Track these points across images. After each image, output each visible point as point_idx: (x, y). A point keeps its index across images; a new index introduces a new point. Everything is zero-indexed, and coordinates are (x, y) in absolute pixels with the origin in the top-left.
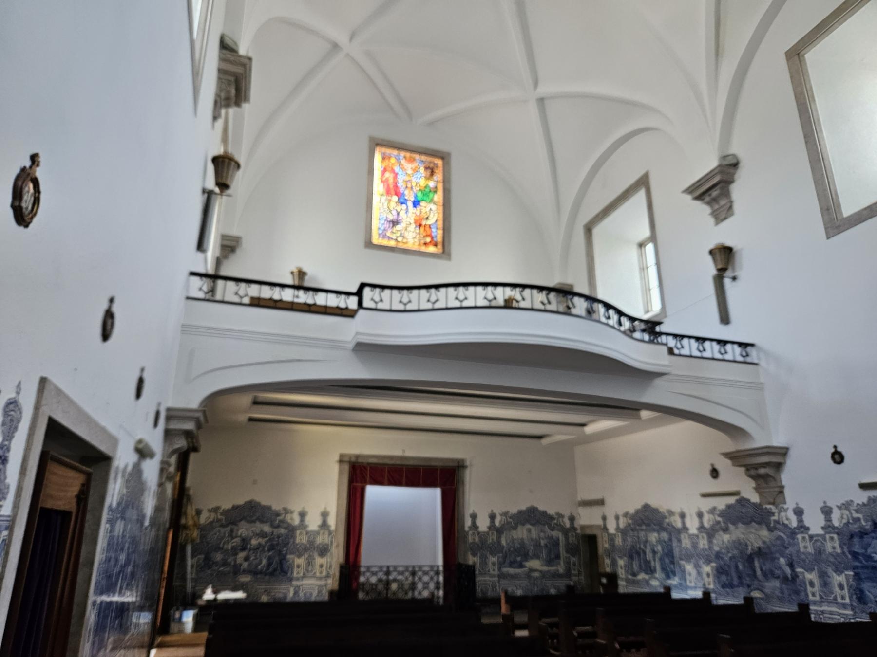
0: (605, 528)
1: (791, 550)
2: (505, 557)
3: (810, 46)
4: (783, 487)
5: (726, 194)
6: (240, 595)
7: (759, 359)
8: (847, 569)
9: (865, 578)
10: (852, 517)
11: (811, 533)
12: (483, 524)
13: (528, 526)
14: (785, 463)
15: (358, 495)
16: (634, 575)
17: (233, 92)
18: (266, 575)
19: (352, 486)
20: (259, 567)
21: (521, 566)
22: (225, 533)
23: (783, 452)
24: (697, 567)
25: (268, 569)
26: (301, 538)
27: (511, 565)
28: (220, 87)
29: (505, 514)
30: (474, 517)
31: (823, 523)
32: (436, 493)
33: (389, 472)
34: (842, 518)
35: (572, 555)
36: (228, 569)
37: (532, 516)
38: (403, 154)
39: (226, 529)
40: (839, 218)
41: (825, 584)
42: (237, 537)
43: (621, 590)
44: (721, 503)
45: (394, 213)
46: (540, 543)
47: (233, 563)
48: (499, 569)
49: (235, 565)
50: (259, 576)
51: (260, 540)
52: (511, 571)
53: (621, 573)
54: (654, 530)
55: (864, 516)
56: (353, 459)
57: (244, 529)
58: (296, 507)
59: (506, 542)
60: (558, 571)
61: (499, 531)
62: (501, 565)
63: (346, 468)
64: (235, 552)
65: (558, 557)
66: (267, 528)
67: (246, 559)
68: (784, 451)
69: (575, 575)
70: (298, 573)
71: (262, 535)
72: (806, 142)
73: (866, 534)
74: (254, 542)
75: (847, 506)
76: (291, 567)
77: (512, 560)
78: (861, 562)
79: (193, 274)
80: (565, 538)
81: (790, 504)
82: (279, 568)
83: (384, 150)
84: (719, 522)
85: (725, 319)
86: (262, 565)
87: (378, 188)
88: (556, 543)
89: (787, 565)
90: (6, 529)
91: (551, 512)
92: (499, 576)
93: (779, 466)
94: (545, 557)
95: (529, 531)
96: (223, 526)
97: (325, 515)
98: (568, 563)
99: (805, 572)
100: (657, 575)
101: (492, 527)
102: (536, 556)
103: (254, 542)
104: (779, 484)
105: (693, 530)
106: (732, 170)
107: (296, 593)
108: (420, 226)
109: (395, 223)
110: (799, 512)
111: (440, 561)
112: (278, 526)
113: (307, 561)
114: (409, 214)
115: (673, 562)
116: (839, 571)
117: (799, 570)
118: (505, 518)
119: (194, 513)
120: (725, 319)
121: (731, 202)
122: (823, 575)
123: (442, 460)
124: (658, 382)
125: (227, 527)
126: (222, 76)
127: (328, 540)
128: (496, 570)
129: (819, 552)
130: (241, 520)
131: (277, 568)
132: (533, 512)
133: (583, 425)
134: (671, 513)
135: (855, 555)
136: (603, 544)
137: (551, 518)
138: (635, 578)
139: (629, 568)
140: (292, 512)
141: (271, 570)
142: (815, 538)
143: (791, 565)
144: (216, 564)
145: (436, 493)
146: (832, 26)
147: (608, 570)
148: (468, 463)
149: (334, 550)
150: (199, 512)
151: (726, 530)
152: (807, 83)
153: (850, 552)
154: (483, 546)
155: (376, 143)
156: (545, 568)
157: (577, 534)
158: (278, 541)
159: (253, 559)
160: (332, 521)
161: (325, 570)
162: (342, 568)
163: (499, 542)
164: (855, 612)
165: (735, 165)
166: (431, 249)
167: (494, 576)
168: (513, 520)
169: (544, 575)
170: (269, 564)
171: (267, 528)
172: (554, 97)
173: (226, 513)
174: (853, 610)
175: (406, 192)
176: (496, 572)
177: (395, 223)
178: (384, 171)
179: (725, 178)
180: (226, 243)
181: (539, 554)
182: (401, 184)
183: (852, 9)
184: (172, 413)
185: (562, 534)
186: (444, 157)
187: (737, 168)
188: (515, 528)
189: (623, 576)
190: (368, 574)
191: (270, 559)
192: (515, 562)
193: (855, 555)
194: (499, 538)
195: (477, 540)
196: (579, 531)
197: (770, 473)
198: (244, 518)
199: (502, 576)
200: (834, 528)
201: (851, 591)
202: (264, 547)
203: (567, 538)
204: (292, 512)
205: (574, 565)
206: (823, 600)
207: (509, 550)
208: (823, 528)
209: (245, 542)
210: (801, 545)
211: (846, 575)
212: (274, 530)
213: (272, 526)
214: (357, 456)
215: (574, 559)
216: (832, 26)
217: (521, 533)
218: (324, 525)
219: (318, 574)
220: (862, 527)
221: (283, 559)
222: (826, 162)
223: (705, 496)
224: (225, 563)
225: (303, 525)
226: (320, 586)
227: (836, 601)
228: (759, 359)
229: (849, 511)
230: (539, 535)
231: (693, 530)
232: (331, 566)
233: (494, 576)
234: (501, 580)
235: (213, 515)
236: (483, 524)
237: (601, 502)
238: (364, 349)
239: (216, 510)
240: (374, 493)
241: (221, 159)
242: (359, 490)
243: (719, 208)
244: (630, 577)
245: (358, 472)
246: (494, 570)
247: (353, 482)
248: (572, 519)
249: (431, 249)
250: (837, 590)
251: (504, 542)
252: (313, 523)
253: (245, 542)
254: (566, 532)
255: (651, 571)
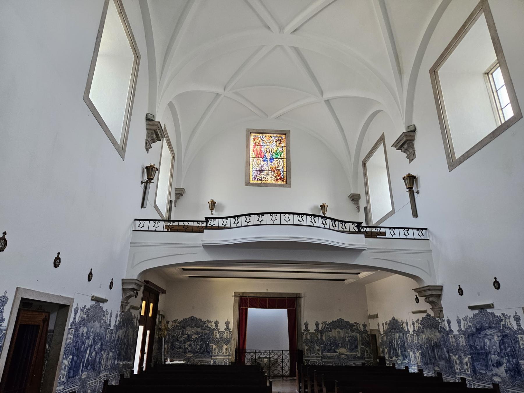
0: (379, 331)
1: (447, 343)
2: (325, 347)
3: (439, 67)
4: (442, 308)
5: (412, 147)
6: (182, 362)
7: (429, 236)
8: (468, 355)
9: (475, 360)
10: (468, 325)
11: (310, 332)
12: (312, 328)
13: (338, 330)
14: (442, 294)
15: (244, 313)
16: (392, 358)
17: (155, 136)
18: (199, 353)
19: (240, 309)
20: (196, 350)
21: (335, 352)
22: (180, 333)
23: (441, 288)
24: (414, 353)
25: (199, 351)
26: (216, 335)
27: (329, 351)
28: (148, 136)
29: (325, 323)
30: (306, 324)
31: (458, 328)
32: (284, 312)
33: (259, 301)
34: (465, 326)
35: (365, 346)
36: (182, 351)
37: (340, 324)
38: (264, 135)
39: (180, 331)
40: (453, 161)
41: (461, 363)
42: (185, 334)
43: (387, 365)
44: (421, 316)
45: (260, 166)
46: (346, 340)
47: (184, 348)
48: (322, 353)
49: (185, 348)
50: (196, 354)
51: (196, 336)
52: (329, 354)
53: (386, 356)
54: (397, 332)
55: (472, 324)
56: (241, 295)
57: (189, 331)
58: (213, 320)
59: (326, 338)
60: (357, 355)
61: (322, 332)
62: (322, 351)
63: (238, 298)
64: (184, 342)
65: (357, 347)
66: (199, 330)
67: (190, 345)
68: (441, 288)
69: (368, 358)
70: (215, 353)
71: (198, 333)
72: (439, 119)
73: (474, 335)
74: (193, 337)
75: (465, 319)
76: (211, 350)
77: (329, 349)
78: (473, 351)
79: (136, 220)
80: (361, 337)
81: (445, 318)
82: (205, 350)
83: (254, 134)
84: (470, 326)
85: (415, 214)
86: (198, 348)
87: (252, 154)
88: (356, 339)
89: (447, 352)
90: (5, 330)
91: (352, 322)
92: (322, 357)
93: (439, 296)
94: (349, 347)
95: (339, 332)
96: (178, 329)
97: (227, 323)
98: (363, 351)
99: (453, 356)
100: (400, 358)
101: (317, 330)
102: (344, 347)
103: (193, 337)
104: (440, 306)
105: (456, 332)
106: (412, 134)
107: (214, 363)
108: (274, 171)
109: (260, 171)
110: (449, 322)
111: (288, 348)
112: (205, 329)
113: (219, 347)
114: (268, 166)
115: (405, 350)
116: (465, 355)
117: (451, 355)
118: (324, 325)
119: (165, 322)
120: (415, 214)
121: (414, 151)
122: (460, 358)
123: (288, 294)
124: (363, 253)
125: (181, 330)
126: (148, 131)
127: (229, 337)
128: (320, 354)
129: (221, 338)
130: (187, 326)
131: (205, 350)
132: (341, 322)
133: (358, 274)
134: (403, 322)
135: (471, 346)
136: (379, 341)
137: (352, 325)
138: (392, 359)
139: (389, 352)
140: (212, 322)
141: (202, 351)
142: (311, 334)
143: (448, 352)
144: (176, 348)
145: (284, 312)
146: (445, 57)
147: (382, 355)
148: (303, 295)
149: (232, 341)
150: (168, 322)
151: (423, 332)
152: (438, 86)
153: (469, 345)
154: (312, 340)
155: (251, 132)
156: (348, 353)
157: (368, 334)
158: (205, 337)
159: (193, 346)
160: (231, 326)
161: (228, 352)
162: (236, 350)
163: (321, 339)
164: (473, 379)
165: (415, 131)
166: (280, 182)
167: (319, 357)
168: (330, 327)
169: (348, 357)
170: (201, 348)
171: (199, 330)
172: (333, 99)
173: (180, 322)
174: (472, 377)
175: (267, 154)
176: (320, 355)
177: (260, 171)
178: (255, 145)
179: (409, 138)
180: (178, 192)
181: (346, 346)
182: (264, 151)
183: (452, 48)
184: (124, 281)
185: (359, 335)
186: (286, 133)
187: (416, 132)
188: (331, 331)
189: (388, 359)
190: (260, 354)
191: (201, 345)
192: (331, 350)
193: (471, 346)
194: (321, 336)
195: (309, 337)
196: (369, 333)
197: (434, 301)
198: (188, 325)
199: (323, 357)
200: (462, 331)
201: (470, 367)
202: (198, 339)
203: (362, 337)
204: (212, 322)
205: (367, 352)
206: (461, 372)
207: (328, 344)
208: (315, 330)
209: (189, 337)
210: (451, 341)
211: (468, 357)
212: (203, 331)
213: (202, 329)
214: (243, 293)
215: (367, 349)
216: (445, 57)
217: (335, 333)
218: (227, 328)
219: (224, 354)
220: (472, 331)
221: (207, 346)
222: (448, 130)
223: (414, 313)
224: (180, 348)
225: (217, 328)
226: (226, 360)
227: (465, 373)
228: (429, 236)
229: (467, 321)
230: (345, 335)
231: (456, 332)
232: (231, 350)
233: (319, 357)
234: (323, 359)
235: (174, 324)
236: (312, 328)
237: (377, 316)
238: (207, 247)
239: (175, 321)
240: (253, 312)
241: (148, 168)
242: (244, 310)
243: (410, 154)
244: (390, 359)
245: (243, 301)
246: (319, 354)
247: (241, 307)
248: (365, 326)
249: (280, 182)
250: (465, 366)
251: (324, 339)
252: (222, 327)
253: (189, 337)
254: (361, 333)
255: (397, 356)
